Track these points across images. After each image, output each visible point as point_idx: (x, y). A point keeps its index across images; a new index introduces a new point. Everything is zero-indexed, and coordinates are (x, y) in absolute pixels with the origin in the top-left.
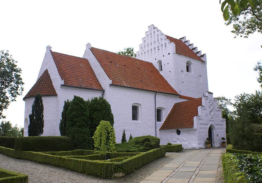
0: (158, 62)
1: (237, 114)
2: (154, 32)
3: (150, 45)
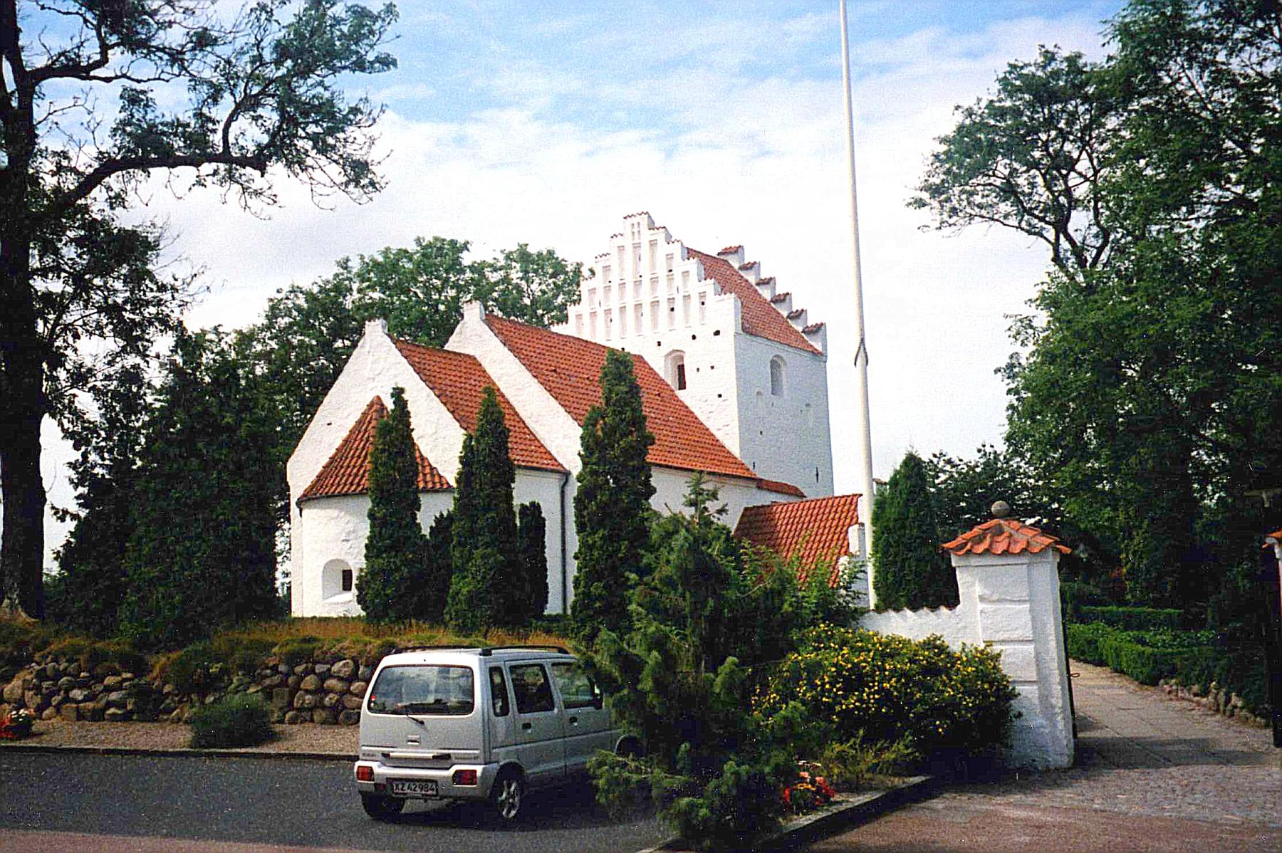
0: (667, 356)
1: (347, 343)
2: (653, 243)
3: (630, 287)
